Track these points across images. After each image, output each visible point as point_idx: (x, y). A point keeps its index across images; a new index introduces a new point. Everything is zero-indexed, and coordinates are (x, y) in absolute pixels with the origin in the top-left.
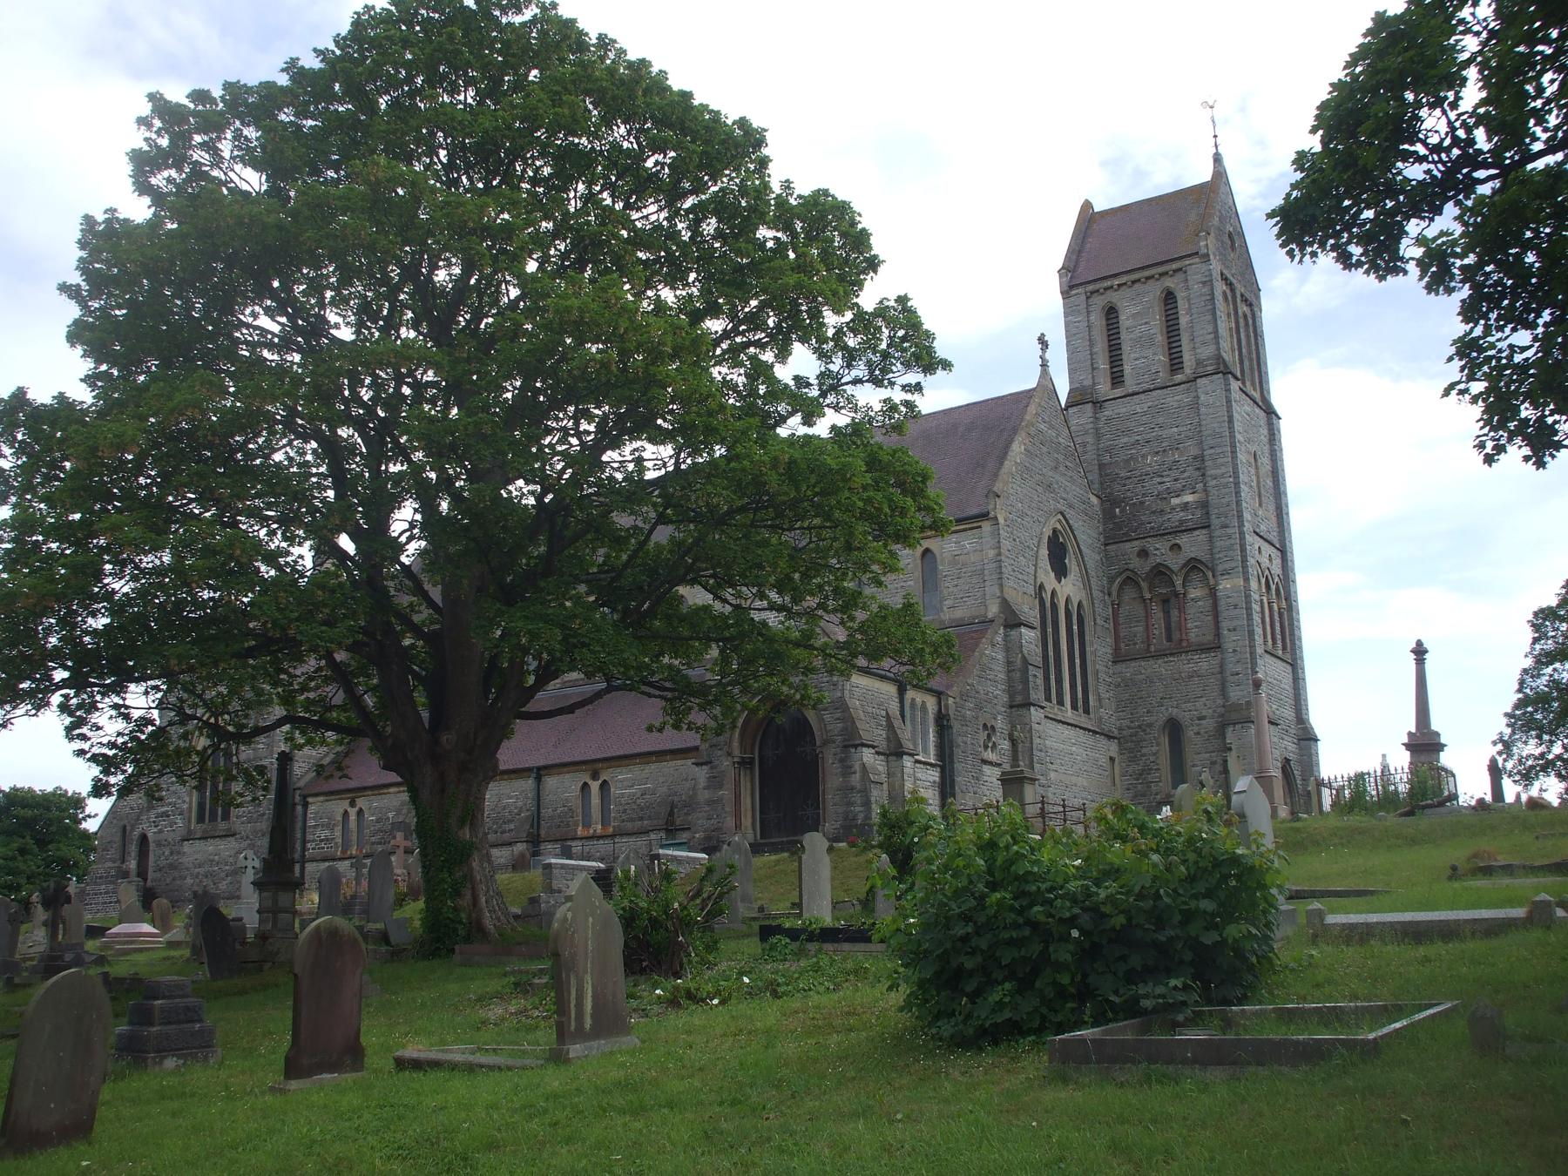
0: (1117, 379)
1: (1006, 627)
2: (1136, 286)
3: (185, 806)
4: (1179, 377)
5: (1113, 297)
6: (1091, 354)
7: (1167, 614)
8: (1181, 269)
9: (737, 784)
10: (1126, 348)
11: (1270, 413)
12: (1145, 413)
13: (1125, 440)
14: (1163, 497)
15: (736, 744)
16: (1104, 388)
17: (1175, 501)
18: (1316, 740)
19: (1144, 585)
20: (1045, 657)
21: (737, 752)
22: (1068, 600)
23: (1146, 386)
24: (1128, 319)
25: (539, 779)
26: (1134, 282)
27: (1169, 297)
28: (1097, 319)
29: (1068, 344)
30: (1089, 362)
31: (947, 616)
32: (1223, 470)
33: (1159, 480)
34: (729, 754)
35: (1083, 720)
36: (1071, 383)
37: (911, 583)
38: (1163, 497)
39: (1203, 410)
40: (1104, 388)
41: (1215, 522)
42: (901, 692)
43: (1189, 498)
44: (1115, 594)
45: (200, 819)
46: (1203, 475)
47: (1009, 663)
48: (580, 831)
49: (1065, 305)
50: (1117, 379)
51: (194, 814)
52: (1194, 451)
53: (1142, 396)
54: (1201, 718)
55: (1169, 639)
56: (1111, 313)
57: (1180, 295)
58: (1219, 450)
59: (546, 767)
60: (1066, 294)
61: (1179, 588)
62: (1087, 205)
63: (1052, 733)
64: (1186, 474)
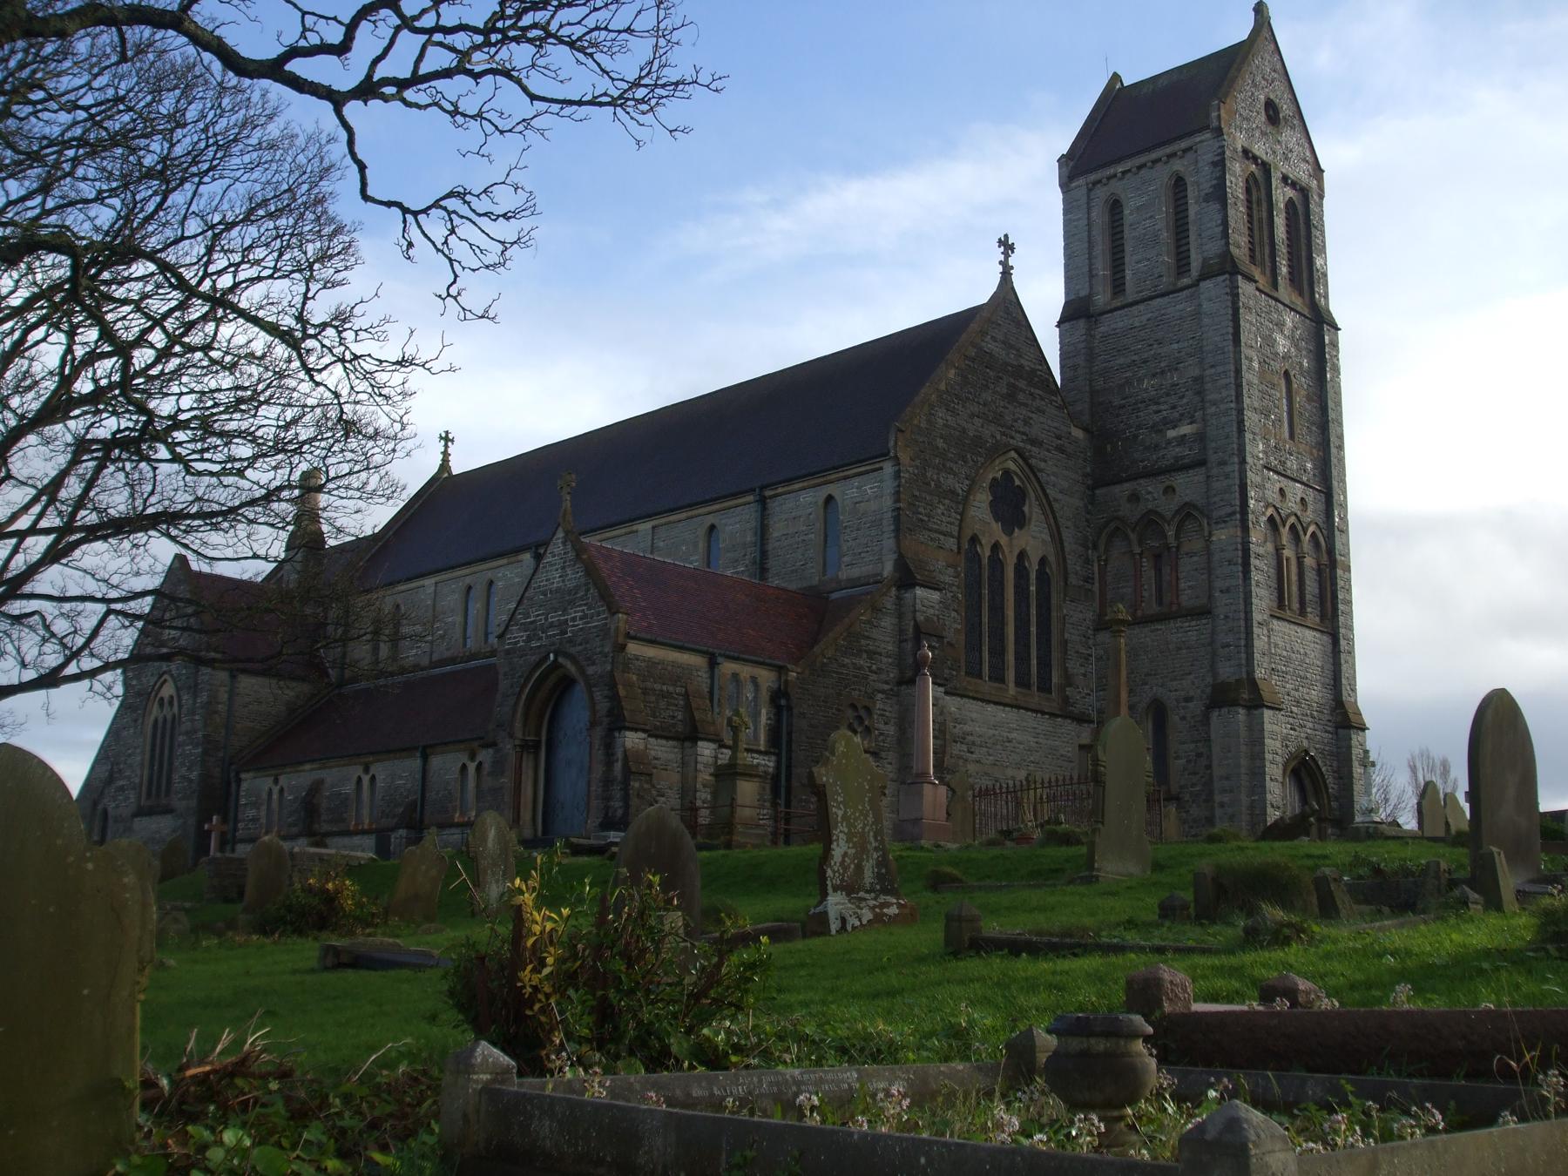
0: (1118, 286)
1: (899, 588)
2: (1143, 172)
3: (137, 780)
4: (1186, 281)
5: (1116, 187)
6: (1090, 259)
7: (1158, 571)
8: (1191, 148)
9: (519, 771)
10: (1128, 248)
11: (1320, 325)
12: (1144, 327)
13: (1121, 361)
14: (1158, 429)
15: (518, 725)
16: (1102, 298)
17: (1171, 434)
18: (1363, 728)
19: (1133, 536)
20: (973, 628)
21: (519, 734)
22: (1022, 555)
23: (1145, 294)
24: (1131, 214)
25: (425, 758)
26: (1140, 168)
27: (1179, 183)
28: (1100, 216)
29: (1066, 248)
30: (1086, 269)
31: (845, 574)
32: (1225, 393)
33: (1155, 408)
34: (511, 736)
35: (1036, 698)
36: (1067, 294)
37: (812, 536)
38: (1158, 429)
39: (1206, 321)
40: (1102, 298)
41: (1213, 458)
42: (713, 664)
43: (1186, 429)
44: (1102, 548)
45: (149, 794)
46: (1202, 401)
47: (901, 631)
48: (457, 818)
49: (1065, 201)
50: (1118, 286)
51: (144, 789)
52: (1197, 372)
53: (1141, 307)
54: (1188, 699)
55: (1160, 602)
56: (1115, 207)
57: (1190, 180)
58: (1220, 369)
59: (431, 746)
60: (1066, 185)
61: (1172, 541)
62: (1116, 77)
63: (974, 715)
64: (1185, 401)
